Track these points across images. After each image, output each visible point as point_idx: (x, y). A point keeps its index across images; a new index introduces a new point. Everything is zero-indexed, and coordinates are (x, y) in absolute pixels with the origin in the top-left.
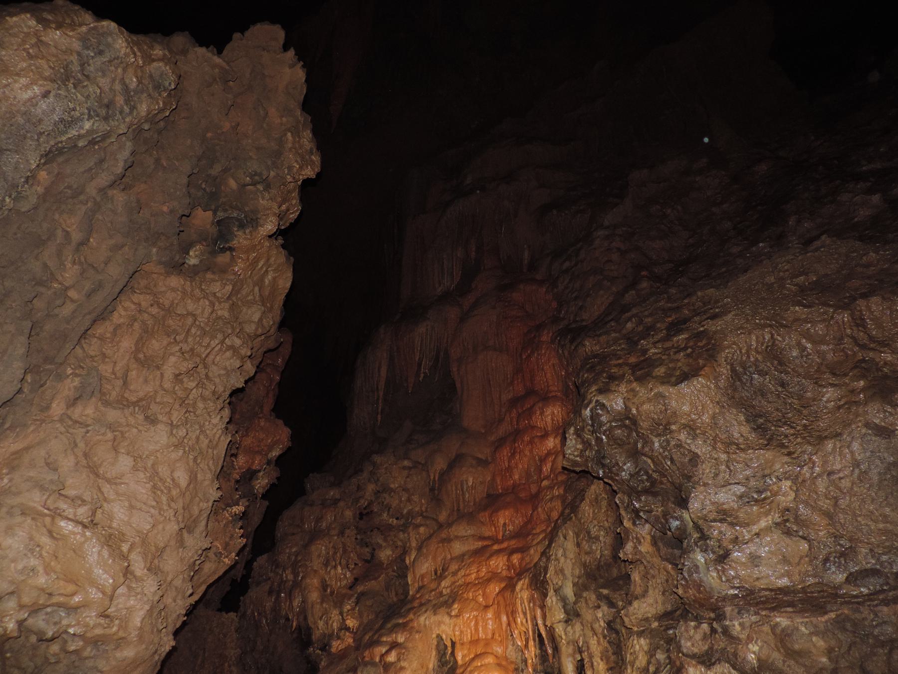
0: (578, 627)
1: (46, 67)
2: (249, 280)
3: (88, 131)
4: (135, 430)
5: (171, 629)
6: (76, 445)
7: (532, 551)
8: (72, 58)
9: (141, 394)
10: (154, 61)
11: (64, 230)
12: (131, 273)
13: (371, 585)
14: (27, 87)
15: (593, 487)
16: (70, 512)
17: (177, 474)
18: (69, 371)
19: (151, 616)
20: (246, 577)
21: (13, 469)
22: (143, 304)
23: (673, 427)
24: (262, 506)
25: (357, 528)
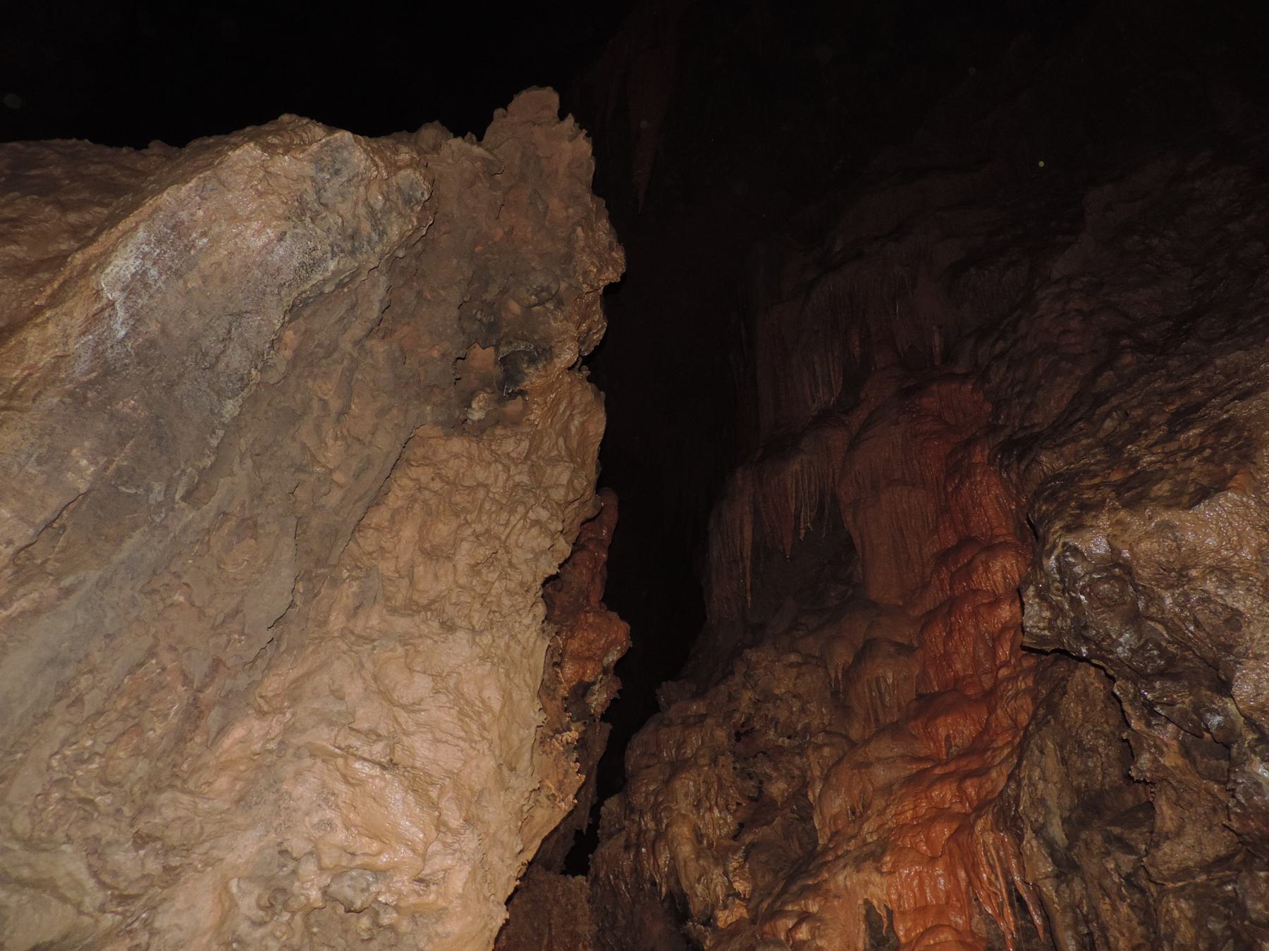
0: (1077, 886)
1: (278, 203)
2: (550, 430)
3: (333, 273)
4: (429, 642)
5: (502, 897)
6: (362, 666)
7: (994, 774)
8: (305, 186)
9: (432, 594)
10: (400, 168)
11: (321, 399)
12: (403, 441)
13: (762, 832)
14: (259, 232)
15: (1078, 673)
16: (364, 750)
17: (486, 694)
18: (345, 574)
19: (474, 880)
20: (594, 827)
21: (295, 700)
22: (424, 479)
23: (1194, 573)
24: (603, 731)
25: (733, 753)
